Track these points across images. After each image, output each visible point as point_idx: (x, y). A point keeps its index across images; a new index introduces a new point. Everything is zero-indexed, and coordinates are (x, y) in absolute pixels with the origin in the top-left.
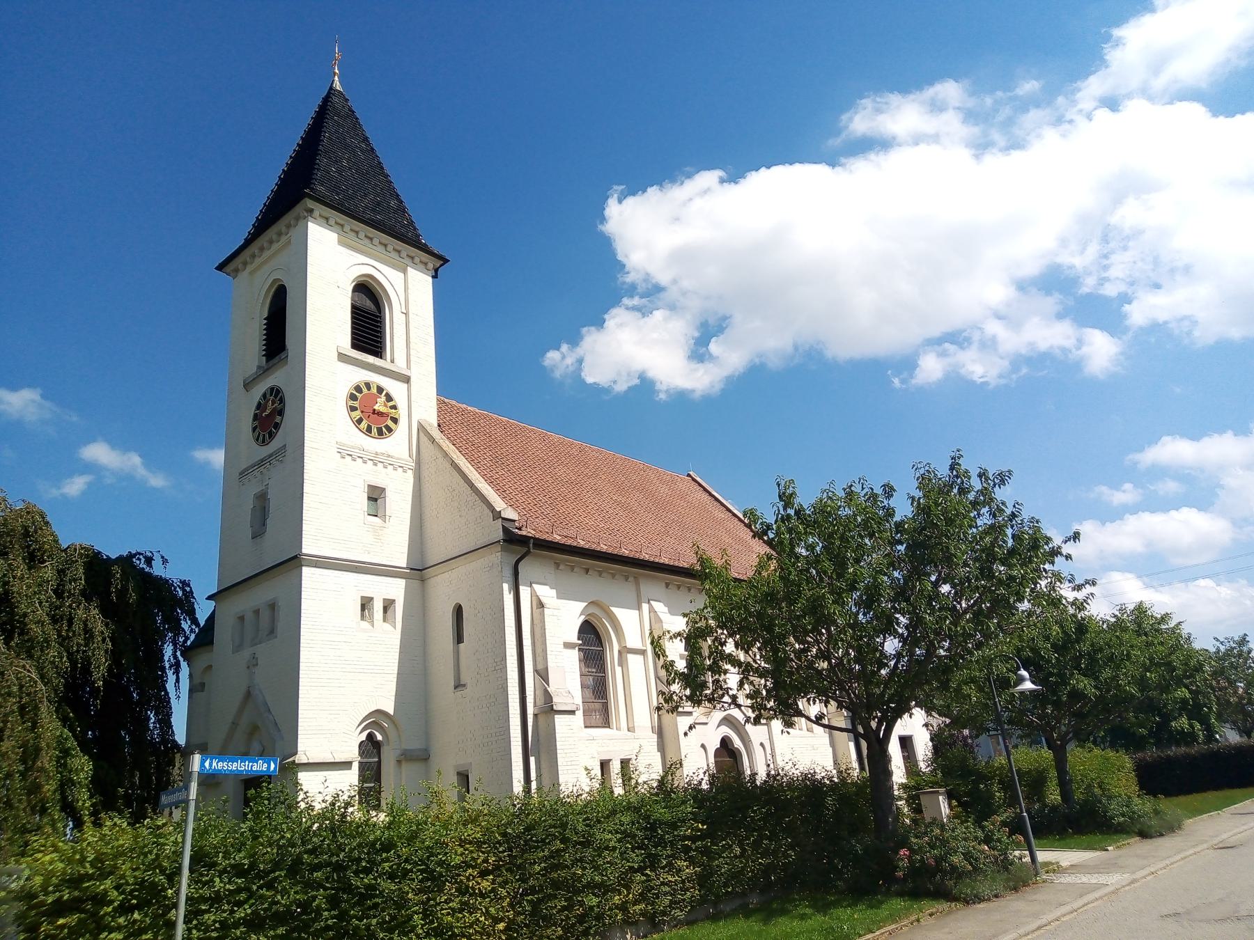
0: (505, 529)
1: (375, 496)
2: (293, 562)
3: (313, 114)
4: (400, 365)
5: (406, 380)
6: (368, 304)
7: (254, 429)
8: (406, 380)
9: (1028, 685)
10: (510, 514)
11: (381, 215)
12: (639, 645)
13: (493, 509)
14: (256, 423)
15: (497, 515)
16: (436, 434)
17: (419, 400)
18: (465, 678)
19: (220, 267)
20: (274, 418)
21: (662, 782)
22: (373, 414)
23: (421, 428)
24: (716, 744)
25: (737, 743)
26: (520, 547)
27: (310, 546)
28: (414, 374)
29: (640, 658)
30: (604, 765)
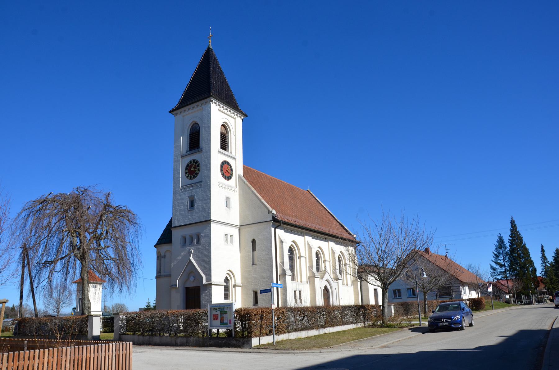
0: (273, 217)
1: (227, 201)
2: (208, 221)
3: (229, 84)
4: (233, 154)
5: (235, 159)
6: (224, 131)
7: (186, 173)
8: (235, 159)
9: (425, 276)
10: (274, 212)
11: (230, 102)
12: (304, 256)
13: (269, 210)
14: (187, 171)
15: (270, 212)
16: (244, 179)
17: (238, 168)
18: (256, 262)
19: (171, 112)
20: (196, 171)
21: (92, 315)
22: (227, 171)
23: (239, 177)
24: (323, 288)
25: (329, 288)
26: (277, 223)
27: (212, 218)
28: (237, 158)
29: (304, 259)
30: (295, 292)
